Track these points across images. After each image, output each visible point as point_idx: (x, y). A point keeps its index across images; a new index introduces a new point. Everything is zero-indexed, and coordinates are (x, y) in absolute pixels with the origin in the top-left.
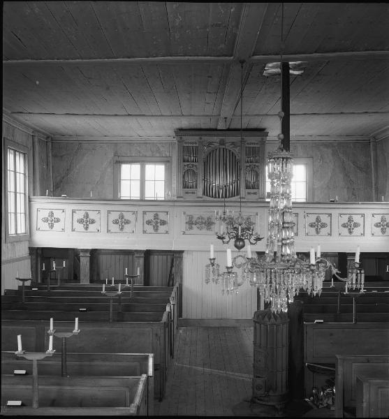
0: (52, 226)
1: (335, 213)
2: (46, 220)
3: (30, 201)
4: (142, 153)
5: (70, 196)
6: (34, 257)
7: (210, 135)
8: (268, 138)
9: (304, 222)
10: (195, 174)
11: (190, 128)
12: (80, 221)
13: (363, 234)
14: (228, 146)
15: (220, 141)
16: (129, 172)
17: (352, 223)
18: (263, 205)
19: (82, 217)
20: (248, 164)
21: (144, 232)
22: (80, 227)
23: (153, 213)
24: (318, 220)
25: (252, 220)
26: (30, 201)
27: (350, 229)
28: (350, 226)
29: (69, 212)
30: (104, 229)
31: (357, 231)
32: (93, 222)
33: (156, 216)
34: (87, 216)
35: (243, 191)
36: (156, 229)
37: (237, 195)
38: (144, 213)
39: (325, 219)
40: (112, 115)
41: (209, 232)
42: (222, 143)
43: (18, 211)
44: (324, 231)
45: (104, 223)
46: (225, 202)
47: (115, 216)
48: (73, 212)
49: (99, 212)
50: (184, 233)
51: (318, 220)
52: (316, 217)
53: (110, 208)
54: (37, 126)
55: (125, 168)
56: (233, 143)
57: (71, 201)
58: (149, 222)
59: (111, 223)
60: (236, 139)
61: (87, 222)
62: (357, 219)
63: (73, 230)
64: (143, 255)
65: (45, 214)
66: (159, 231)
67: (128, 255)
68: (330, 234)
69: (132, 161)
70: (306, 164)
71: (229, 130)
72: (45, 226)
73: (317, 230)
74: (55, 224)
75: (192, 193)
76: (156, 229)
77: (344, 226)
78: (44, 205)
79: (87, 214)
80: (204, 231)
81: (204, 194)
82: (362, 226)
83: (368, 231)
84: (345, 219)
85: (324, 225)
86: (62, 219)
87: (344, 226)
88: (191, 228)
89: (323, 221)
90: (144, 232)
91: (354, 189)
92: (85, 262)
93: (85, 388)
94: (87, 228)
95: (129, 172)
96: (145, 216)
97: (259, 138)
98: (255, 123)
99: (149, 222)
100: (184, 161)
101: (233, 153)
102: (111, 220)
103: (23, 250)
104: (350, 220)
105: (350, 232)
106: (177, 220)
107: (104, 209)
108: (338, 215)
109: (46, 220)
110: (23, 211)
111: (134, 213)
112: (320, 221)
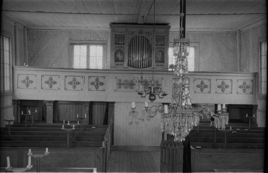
0: (28, 86)
2: (24, 82)
6: (16, 106)
13: (231, 93)
16: (79, 51)
21: (90, 90)
23: (96, 78)
24: (202, 83)
28: (223, 87)
29: (39, 77)
30: (62, 89)
31: (227, 90)
32: (55, 83)
33: (97, 80)
36: (97, 88)
39: (206, 82)
41: (131, 90)
42: (140, 32)
44: (206, 90)
46: (142, 71)
47: (70, 79)
48: (42, 76)
49: (60, 78)
50: (115, 91)
51: (202, 83)
58: (92, 84)
61: (51, 83)
62: (228, 83)
65: (22, 78)
66: (76, 89)
71: (145, 24)
72: (23, 85)
73: (222, 89)
76: (97, 88)
79: (51, 78)
80: (129, 89)
82: (230, 87)
83: (234, 91)
84: (220, 83)
85: (206, 86)
87: (198, 86)
88: (120, 87)
90: (90, 90)
94: (51, 87)
95: (79, 51)
99: (92, 84)
100: (116, 44)
101: (147, 39)
106: (111, 83)
107: (62, 75)
109: (24, 82)
110: (8, 76)
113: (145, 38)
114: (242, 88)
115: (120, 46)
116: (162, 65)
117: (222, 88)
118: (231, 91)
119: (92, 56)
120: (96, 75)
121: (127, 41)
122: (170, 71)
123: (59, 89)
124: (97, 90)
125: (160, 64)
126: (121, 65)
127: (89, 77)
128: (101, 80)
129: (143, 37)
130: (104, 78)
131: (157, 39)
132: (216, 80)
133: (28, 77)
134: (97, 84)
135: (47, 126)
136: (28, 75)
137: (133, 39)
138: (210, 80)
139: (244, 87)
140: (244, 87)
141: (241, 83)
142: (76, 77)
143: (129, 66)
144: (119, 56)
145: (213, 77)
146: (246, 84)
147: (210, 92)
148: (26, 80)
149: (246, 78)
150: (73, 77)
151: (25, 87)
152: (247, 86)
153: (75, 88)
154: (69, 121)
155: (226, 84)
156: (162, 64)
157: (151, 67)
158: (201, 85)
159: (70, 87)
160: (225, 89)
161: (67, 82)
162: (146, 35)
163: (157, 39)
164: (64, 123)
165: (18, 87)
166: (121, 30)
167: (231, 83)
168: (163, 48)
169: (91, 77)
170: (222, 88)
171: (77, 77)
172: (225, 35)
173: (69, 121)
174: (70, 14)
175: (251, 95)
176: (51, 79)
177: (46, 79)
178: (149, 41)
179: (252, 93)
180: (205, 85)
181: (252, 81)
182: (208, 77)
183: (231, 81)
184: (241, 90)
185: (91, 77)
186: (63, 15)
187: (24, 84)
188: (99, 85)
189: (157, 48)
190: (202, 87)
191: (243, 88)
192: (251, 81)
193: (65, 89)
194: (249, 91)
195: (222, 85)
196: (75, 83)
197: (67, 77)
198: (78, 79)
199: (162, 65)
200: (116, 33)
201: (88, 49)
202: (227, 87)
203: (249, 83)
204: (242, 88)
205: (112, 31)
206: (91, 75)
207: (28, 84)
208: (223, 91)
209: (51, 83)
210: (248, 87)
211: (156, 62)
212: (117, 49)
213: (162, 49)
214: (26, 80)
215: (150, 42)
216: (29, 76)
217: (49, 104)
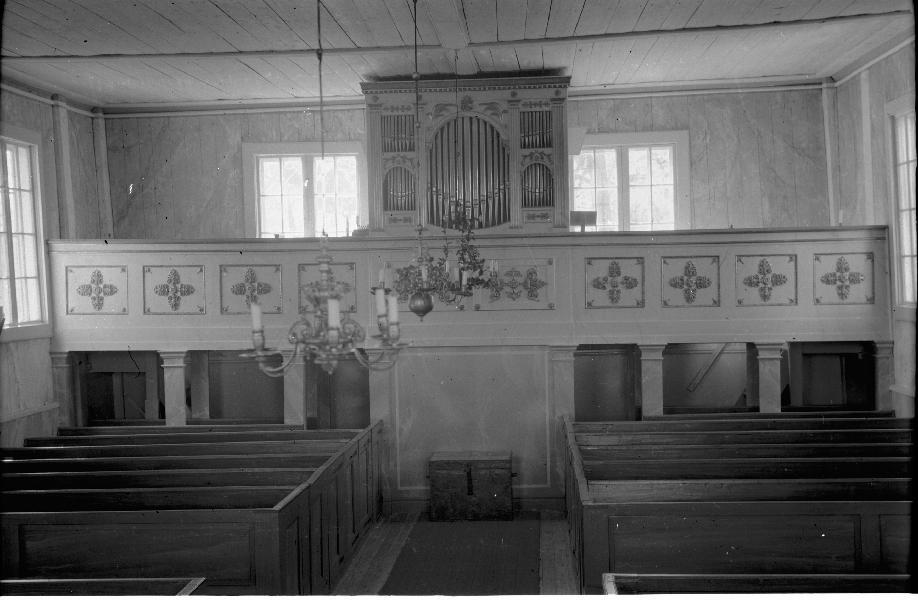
1: (805, 252)
2: (85, 290)
3: (49, 252)
4: (310, 133)
8: (570, 89)
10: (408, 177)
11: (393, 73)
12: (163, 291)
13: (795, 301)
14: (479, 111)
15: (463, 102)
17: (693, 279)
18: (563, 241)
19: (164, 281)
20: (527, 152)
22: (164, 303)
25: (540, 277)
26: (49, 252)
27: (840, 288)
29: (135, 270)
30: (213, 310)
31: (780, 293)
32: (189, 291)
35: (517, 212)
36: (614, 297)
37: (505, 221)
40: (90, 57)
42: (467, 104)
44: (704, 296)
47: (236, 277)
48: (146, 270)
49: (203, 273)
51: (689, 271)
52: (684, 265)
53: (150, 259)
56: (491, 106)
57: (158, 247)
58: (630, 283)
59: (791, 278)
63: (223, 310)
64: (181, 363)
65: (85, 277)
67: (757, 360)
70: (357, 158)
74: (108, 300)
75: (406, 220)
77: (750, 282)
78: (80, 259)
80: (524, 301)
82: (714, 285)
83: (806, 299)
85: (702, 284)
87: (750, 282)
89: (700, 273)
91: (785, 197)
92: (653, 373)
94: (176, 306)
96: (152, 310)
97: (550, 93)
98: (532, 58)
101: (492, 128)
102: (228, 286)
103: (39, 357)
104: (764, 269)
105: (765, 297)
107: (212, 262)
109: (85, 290)
110: (32, 271)
112: (694, 274)
113: (485, 123)
114: (835, 283)
115: (536, 152)
117: (761, 285)
118: (793, 298)
119: (314, 196)
121: (424, 139)
122: (574, 235)
123: (202, 310)
124: (616, 305)
125: (539, 211)
126: (406, 220)
127: (817, 257)
129: (478, 120)
130: (352, 269)
131: (527, 125)
133: (99, 275)
135: (287, 437)
136: (99, 269)
137: (442, 129)
138: (640, 260)
139: (839, 279)
140: (839, 279)
143: (432, 222)
144: (399, 193)
145: (726, 248)
146: (847, 270)
147: (717, 303)
148: (94, 286)
150: (245, 269)
151: (608, 302)
152: (851, 275)
154: (653, 402)
155: (776, 270)
156: (409, 214)
157: (506, 225)
158: (685, 278)
160: (770, 289)
162: (489, 112)
163: (527, 125)
165: (70, 309)
166: (400, 100)
167: (716, 270)
168: (549, 156)
169: (306, 268)
170: (761, 285)
171: (258, 263)
172: (779, 97)
173: (653, 402)
174: (181, 58)
175: (869, 307)
176: (252, 278)
177: (160, 277)
178: (498, 134)
179: (872, 300)
180: (775, 276)
181: (871, 256)
182: (788, 249)
183: (794, 258)
185: (306, 268)
186: (121, 59)
187: (165, 299)
188: (620, 287)
189: (387, 160)
190: (690, 284)
191: (839, 283)
192: (865, 257)
193: (222, 308)
194: (859, 292)
195: (838, 274)
197: (152, 269)
198: (263, 275)
199: (545, 216)
200: (385, 113)
201: (309, 174)
202: (779, 280)
203: (858, 264)
204: (835, 283)
205: (370, 105)
207: (102, 299)
208: (765, 297)
209: (254, 290)
211: (525, 204)
212: (390, 165)
213: (404, 162)
214: (171, 286)
215: (502, 136)
216: (104, 271)
217: (275, 367)
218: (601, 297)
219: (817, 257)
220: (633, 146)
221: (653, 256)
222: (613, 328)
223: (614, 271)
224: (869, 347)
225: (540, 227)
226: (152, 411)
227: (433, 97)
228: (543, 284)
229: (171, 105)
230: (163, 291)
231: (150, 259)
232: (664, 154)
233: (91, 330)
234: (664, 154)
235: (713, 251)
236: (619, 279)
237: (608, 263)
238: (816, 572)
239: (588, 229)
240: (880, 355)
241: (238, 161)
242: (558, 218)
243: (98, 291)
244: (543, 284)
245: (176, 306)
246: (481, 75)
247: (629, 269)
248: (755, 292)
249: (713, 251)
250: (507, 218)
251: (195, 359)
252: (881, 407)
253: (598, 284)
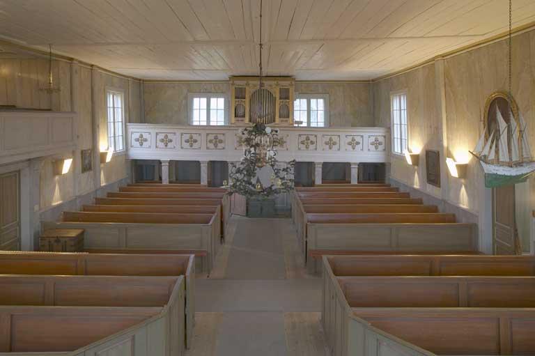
0: (141, 145)
1: (343, 135)
2: (137, 140)
4: (208, 89)
5: (154, 121)
7: (269, 80)
9: (321, 141)
12: (162, 141)
16: (199, 103)
17: (309, 141)
19: (163, 138)
21: (208, 148)
23: (213, 135)
24: (331, 139)
28: (354, 144)
29: (154, 135)
30: (178, 146)
32: (171, 141)
34: (141, 136)
35: (277, 119)
36: (216, 146)
38: (208, 134)
43: (399, 140)
45: (342, 143)
47: (187, 137)
49: (176, 134)
50: (236, 149)
51: (331, 139)
53: (182, 131)
54: (480, 137)
55: (196, 101)
58: (211, 141)
59: (158, 142)
60: (273, 83)
61: (166, 141)
65: (136, 136)
66: (193, 147)
68: (339, 150)
69: (197, 97)
72: (137, 144)
73: (376, 147)
76: (216, 146)
78: (136, 130)
81: (250, 121)
84: (349, 139)
86: (149, 140)
87: (326, 143)
90: (208, 148)
93: (138, 233)
94: (166, 146)
99: (211, 141)
107: (178, 132)
108: (345, 135)
109: (137, 140)
110: (121, 134)
111: (150, 133)
116: (287, 121)
119: (209, 111)
120: (307, 133)
125: (240, 119)
128: (220, 137)
132: (346, 136)
134: (216, 142)
138: (316, 136)
139: (376, 144)
140: (376, 144)
141: (373, 139)
142: (333, 137)
149: (378, 134)
151: (305, 149)
153: (191, 146)
154: (318, 180)
159: (187, 145)
161: (199, 142)
164: (354, 181)
173: (318, 180)
177: (161, 136)
179: (384, 150)
181: (385, 137)
184: (373, 148)
194: (381, 148)
196: (192, 141)
198: (195, 137)
203: (381, 139)
206: (208, 132)
210: (380, 144)
211: (280, 117)
218: (303, 147)
219: (369, 137)
220: (225, 100)
221: (319, 135)
222: (305, 156)
223: (308, 139)
224: (383, 164)
225: (286, 124)
226: (157, 179)
227: (252, 82)
228: (285, 142)
229: (389, 72)
230: (162, 141)
231: (157, 131)
232: (321, 101)
233: (139, 153)
234: (321, 101)
235: (224, 132)
236: (309, 141)
237: (305, 136)
238: (100, 211)
239: (301, 125)
240: (387, 167)
241: (186, 98)
242: (291, 123)
243: (142, 140)
244: (285, 142)
245: (166, 146)
246: (267, 76)
247: (312, 138)
248: (328, 146)
249: (224, 132)
250: (274, 121)
251: (172, 163)
252: (387, 182)
253: (303, 143)
